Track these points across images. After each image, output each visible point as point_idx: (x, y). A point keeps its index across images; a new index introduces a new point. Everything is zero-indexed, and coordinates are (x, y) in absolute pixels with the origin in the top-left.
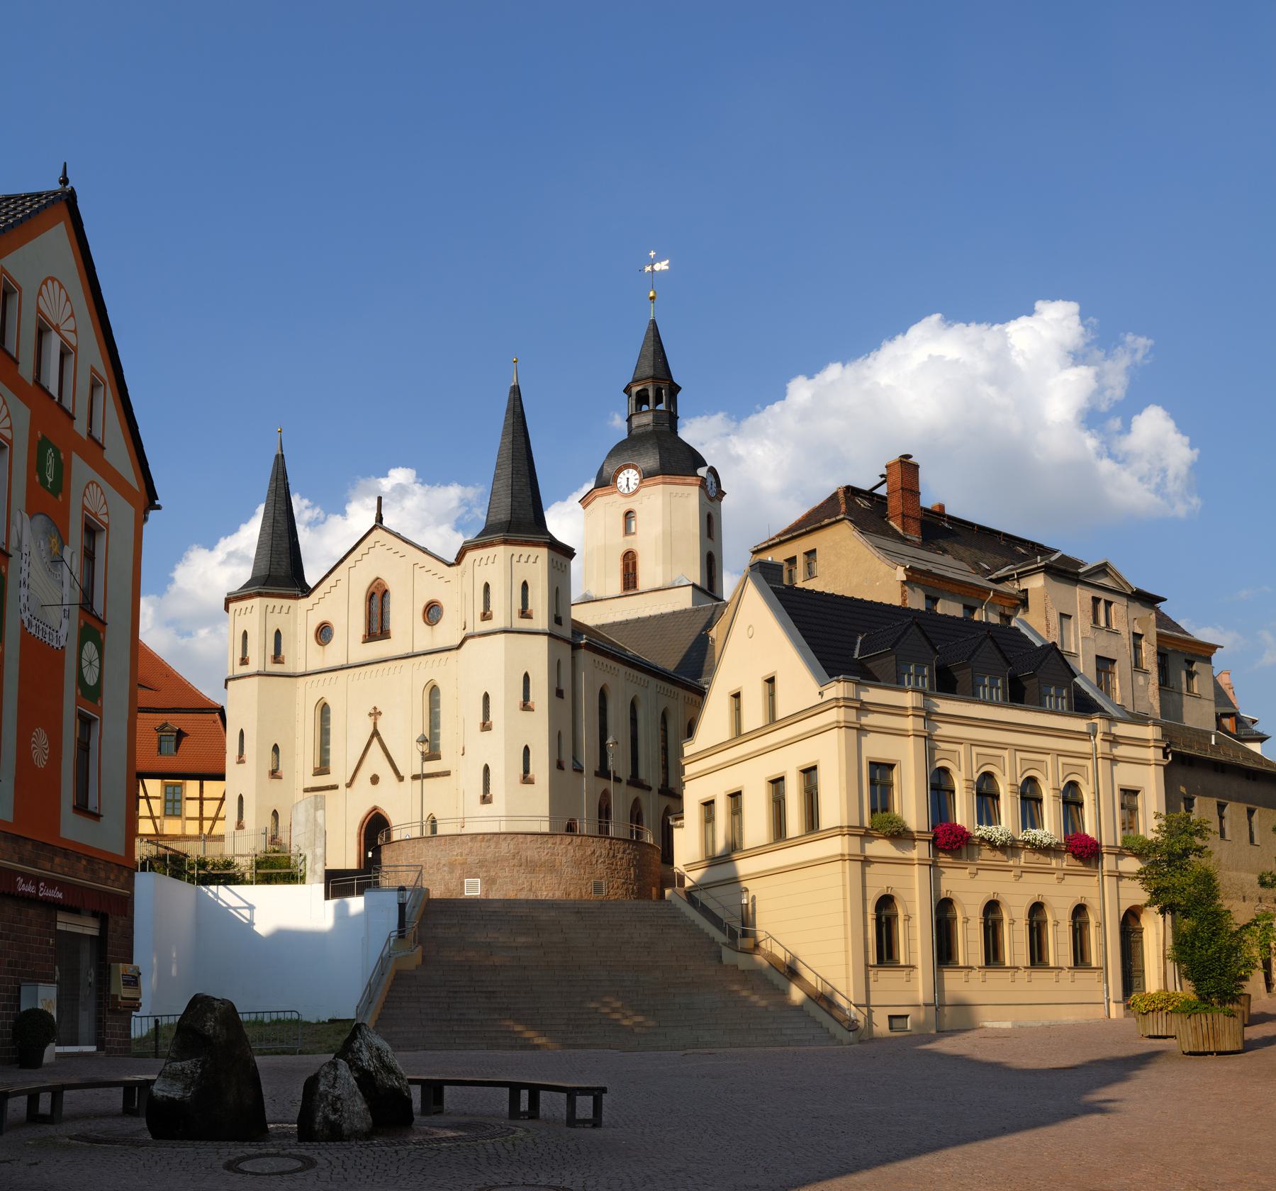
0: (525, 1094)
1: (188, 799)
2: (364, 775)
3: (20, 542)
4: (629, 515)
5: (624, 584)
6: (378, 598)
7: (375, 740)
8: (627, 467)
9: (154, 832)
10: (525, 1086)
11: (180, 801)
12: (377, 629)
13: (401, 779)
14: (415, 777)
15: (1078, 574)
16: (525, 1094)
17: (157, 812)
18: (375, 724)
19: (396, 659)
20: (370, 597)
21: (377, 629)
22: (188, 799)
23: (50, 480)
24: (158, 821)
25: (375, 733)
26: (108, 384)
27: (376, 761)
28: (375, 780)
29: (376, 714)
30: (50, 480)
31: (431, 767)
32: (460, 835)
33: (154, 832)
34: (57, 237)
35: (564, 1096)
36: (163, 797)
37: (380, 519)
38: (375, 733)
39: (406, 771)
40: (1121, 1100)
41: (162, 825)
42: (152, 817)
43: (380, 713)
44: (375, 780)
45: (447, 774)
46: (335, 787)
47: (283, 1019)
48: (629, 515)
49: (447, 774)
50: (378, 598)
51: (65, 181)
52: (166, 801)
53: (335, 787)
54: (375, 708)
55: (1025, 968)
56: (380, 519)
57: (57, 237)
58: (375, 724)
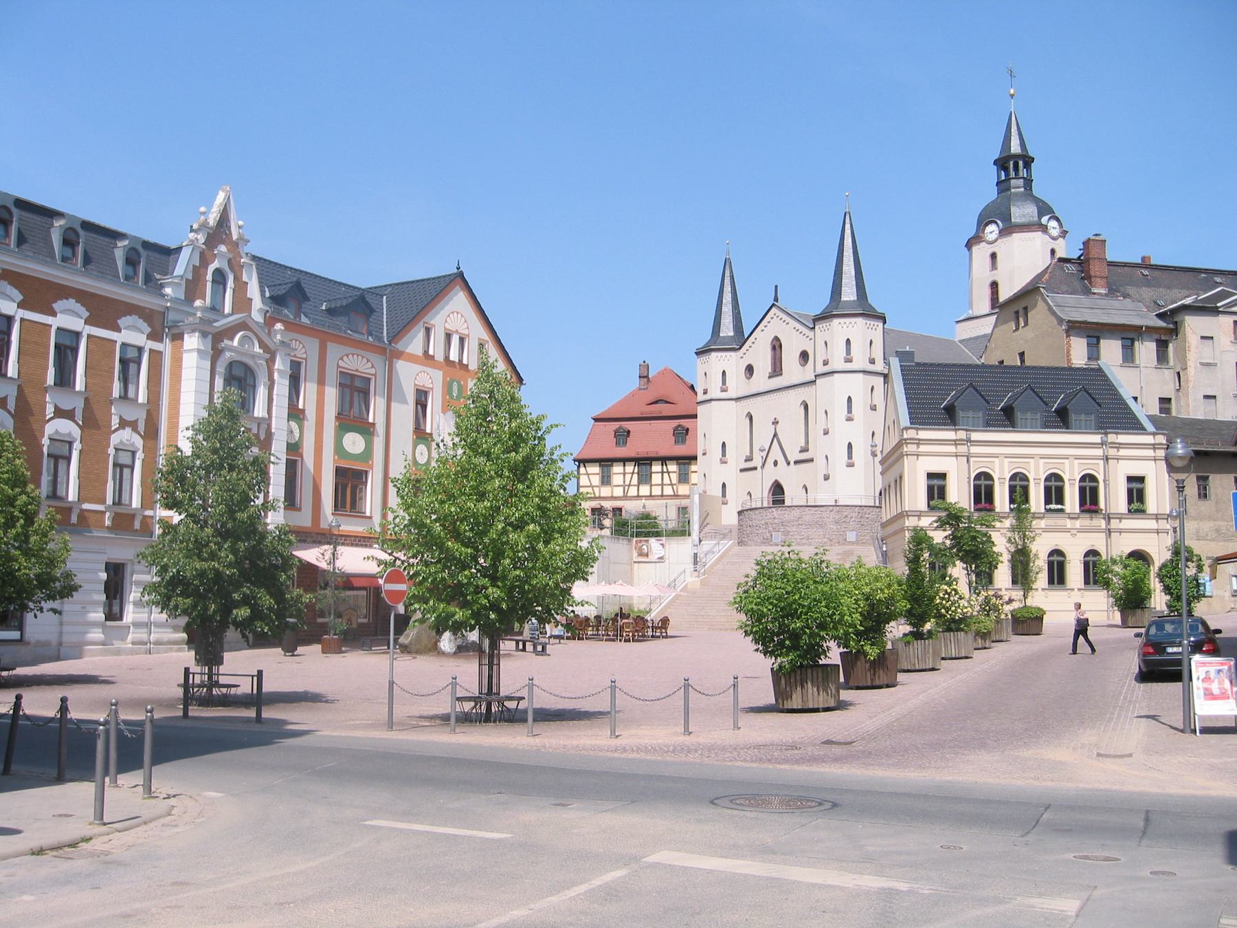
0: (521, 643)
1: (692, 472)
2: (770, 461)
3: (438, 426)
4: (993, 256)
5: (992, 305)
6: (777, 346)
7: (775, 440)
8: (996, 223)
9: (673, 494)
10: (521, 641)
11: (688, 474)
12: (777, 370)
13: (789, 464)
14: (796, 462)
15: (1218, 307)
16: (521, 643)
17: (674, 480)
18: (775, 429)
19: (758, 394)
20: (774, 348)
21: (777, 370)
22: (692, 472)
23: (455, 395)
24: (675, 487)
25: (775, 435)
26: (490, 342)
27: (776, 453)
28: (776, 463)
29: (775, 423)
30: (455, 395)
31: (750, 465)
32: (791, 506)
33: (673, 494)
34: (459, 300)
35: (514, 642)
36: (678, 472)
37: (776, 299)
38: (775, 435)
39: (792, 460)
40: (1159, 716)
41: (677, 489)
42: (672, 485)
43: (777, 422)
44: (776, 463)
45: (812, 460)
46: (755, 468)
47: (154, 607)
48: (993, 256)
49: (812, 460)
50: (777, 346)
51: (458, 268)
52: (679, 474)
53: (755, 468)
54: (775, 419)
55: (1079, 589)
56: (776, 299)
57: (459, 300)
58: (775, 429)
